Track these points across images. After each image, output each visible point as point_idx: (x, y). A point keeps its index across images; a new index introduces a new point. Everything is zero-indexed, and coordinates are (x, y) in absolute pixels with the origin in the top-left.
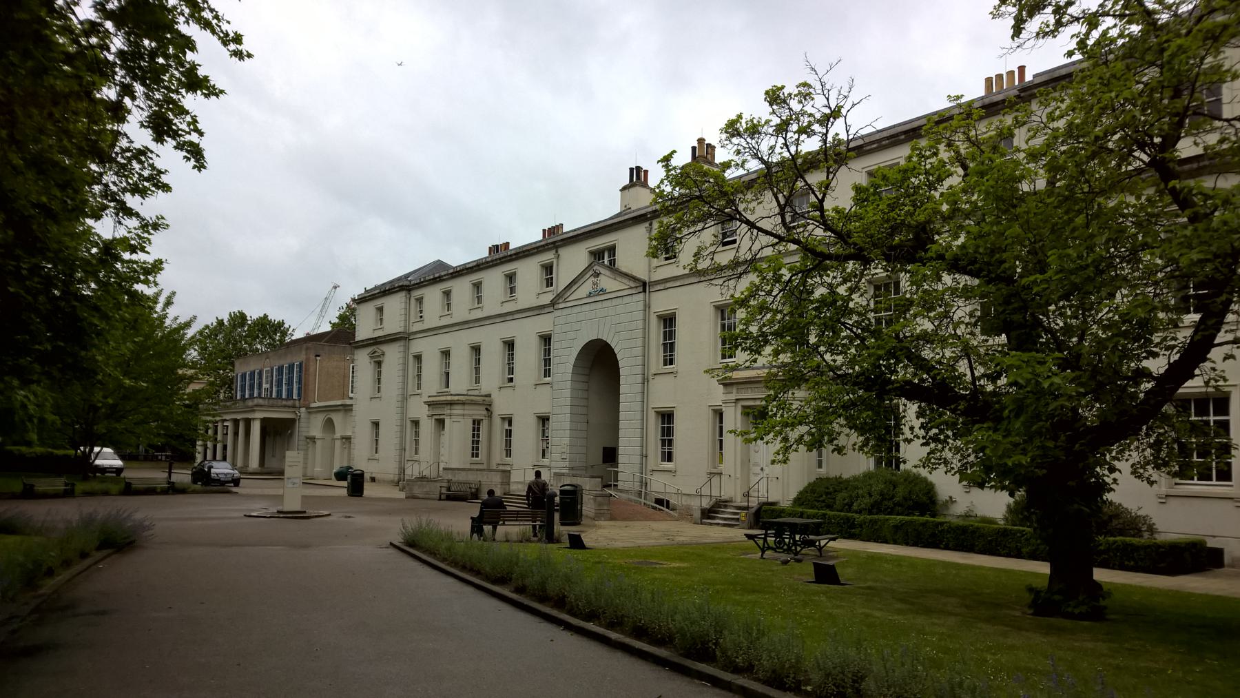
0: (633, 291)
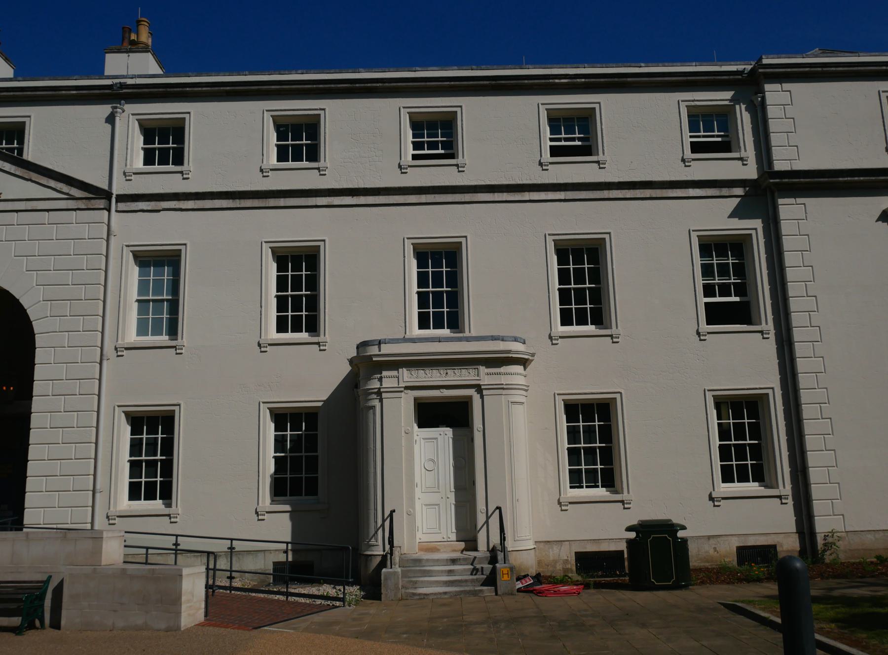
0: (71, 204)
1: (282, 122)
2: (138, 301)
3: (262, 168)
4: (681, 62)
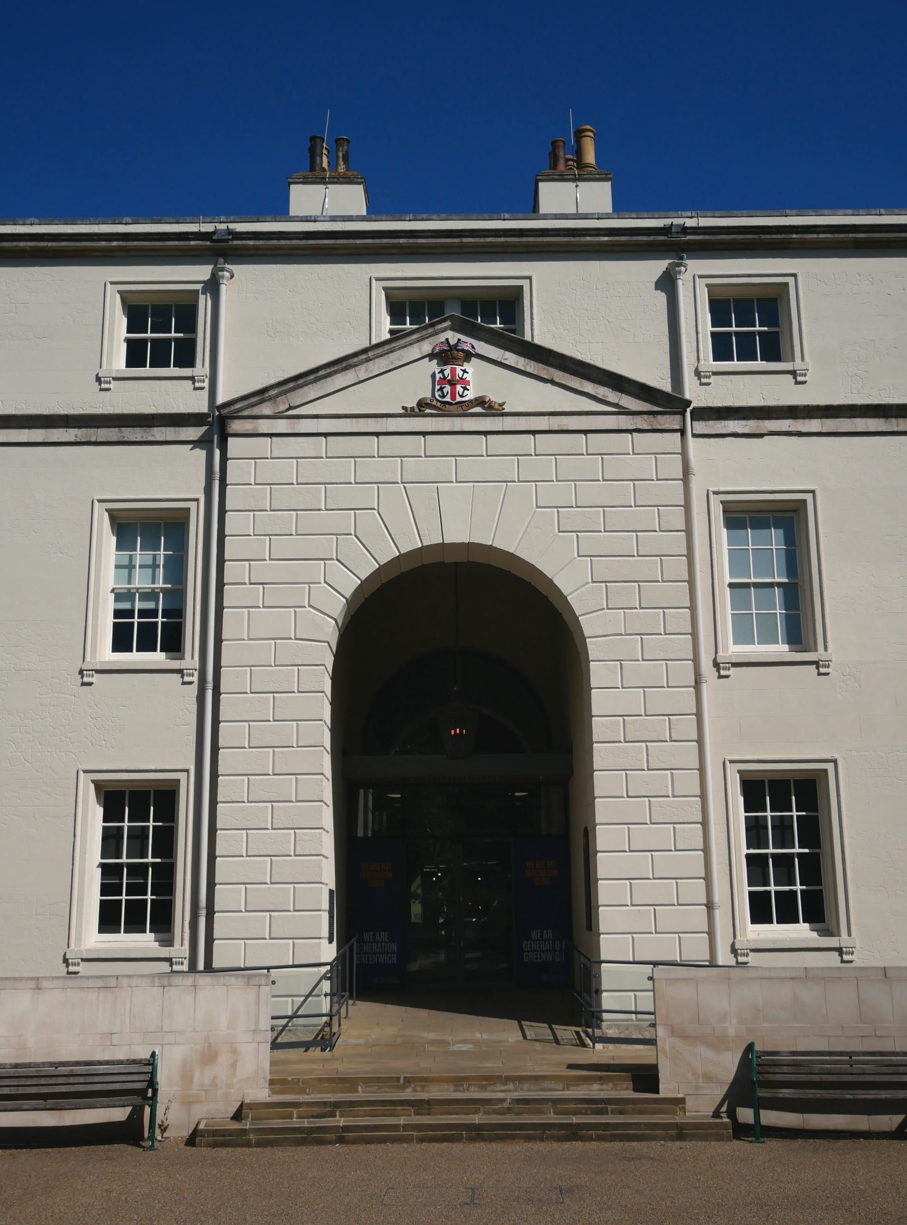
0: (624, 422)
1: (136, 301)
2: (731, 586)
3: (99, 376)
4: (747, 209)
